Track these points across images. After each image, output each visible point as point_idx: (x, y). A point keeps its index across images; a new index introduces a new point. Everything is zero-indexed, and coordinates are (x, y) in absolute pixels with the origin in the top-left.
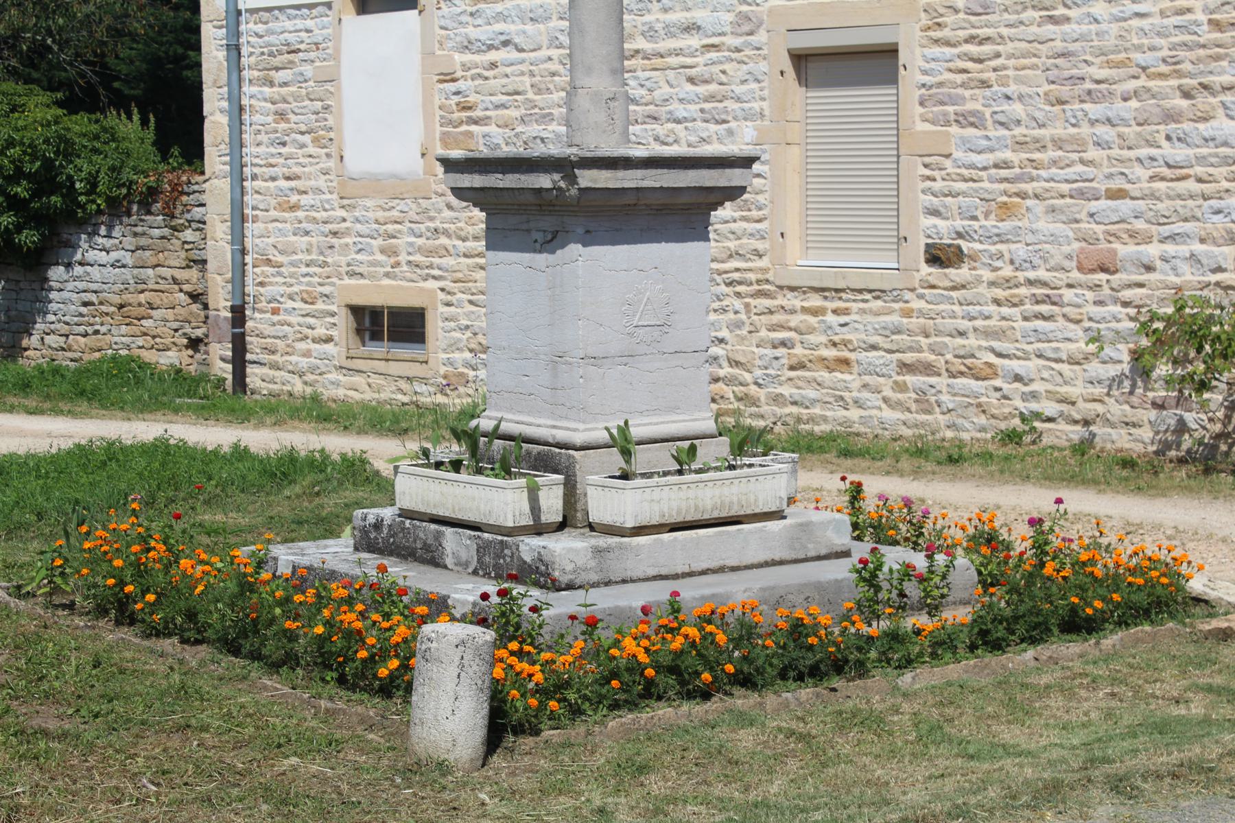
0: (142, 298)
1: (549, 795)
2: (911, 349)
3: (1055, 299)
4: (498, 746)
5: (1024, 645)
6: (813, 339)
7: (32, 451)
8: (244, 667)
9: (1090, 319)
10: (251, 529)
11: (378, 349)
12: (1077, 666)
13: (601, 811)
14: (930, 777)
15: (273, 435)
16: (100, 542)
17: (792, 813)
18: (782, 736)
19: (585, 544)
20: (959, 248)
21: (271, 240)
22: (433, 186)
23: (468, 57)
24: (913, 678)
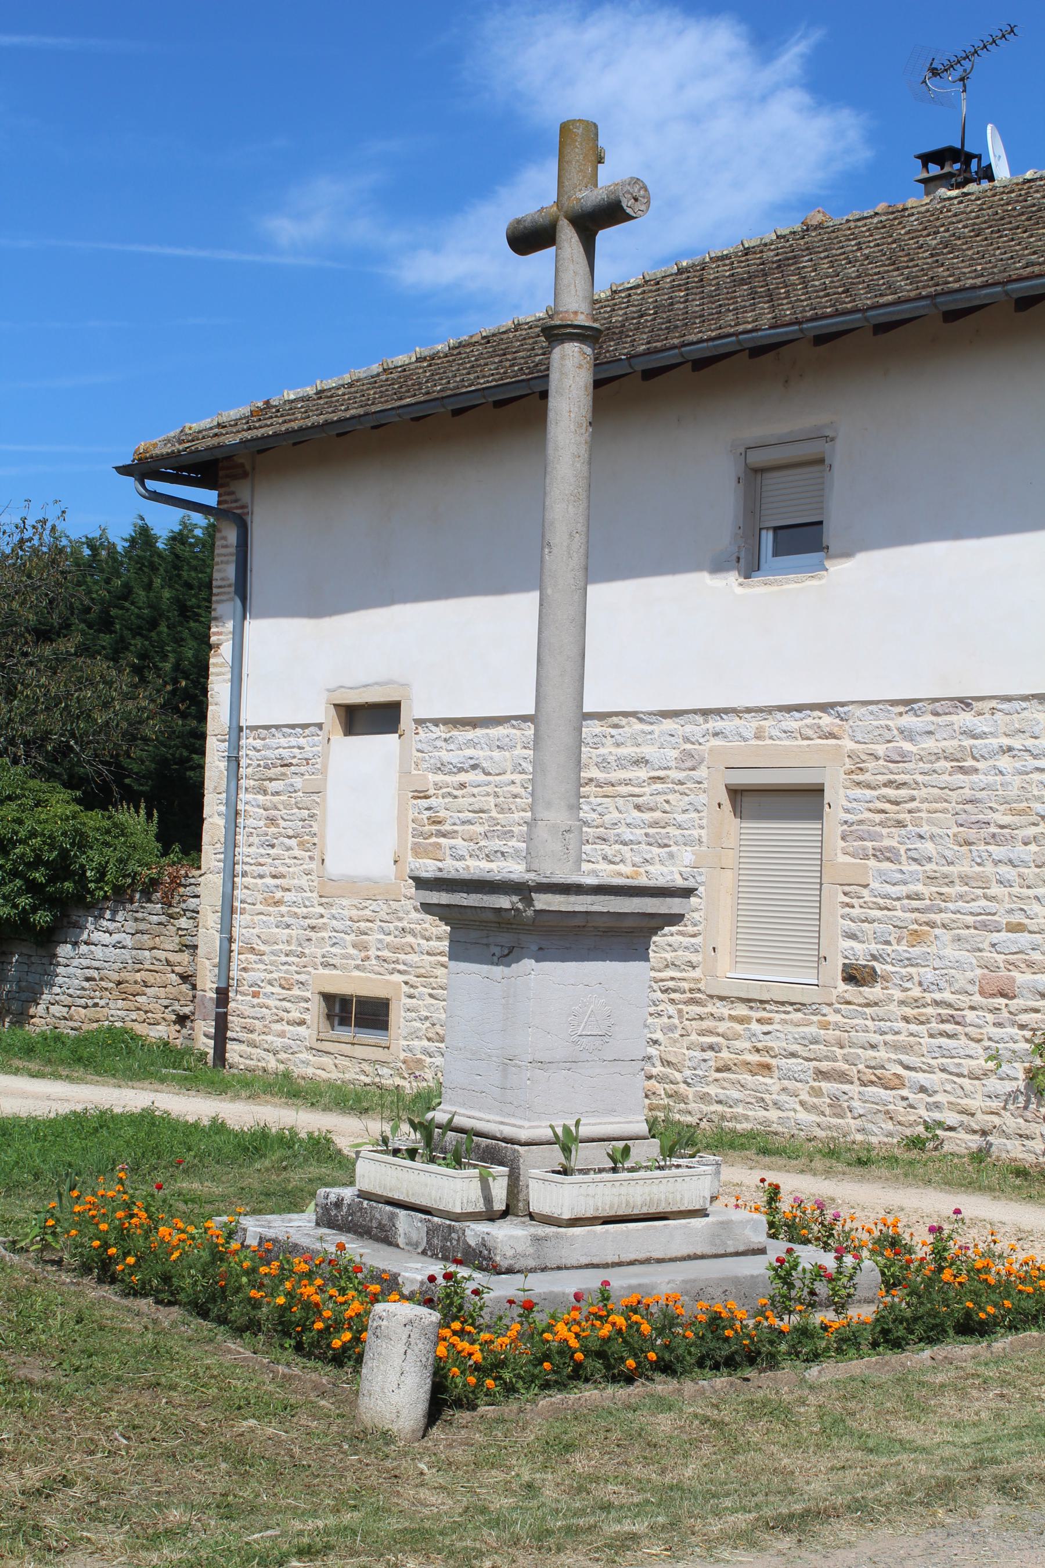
0: (138, 976)
1: (483, 1467)
2: (827, 1058)
3: (959, 1020)
4: (438, 1419)
5: (922, 1344)
6: (738, 1044)
7: (34, 1114)
8: (211, 1330)
9: (990, 1039)
10: (223, 1198)
11: (346, 1033)
12: (970, 1366)
13: (530, 1486)
14: (832, 1469)
15: (247, 1108)
16: (88, 1206)
17: (704, 1498)
18: (697, 1422)
19: (526, 1233)
20: (873, 969)
21: (255, 931)
22: (403, 890)
23: (440, 778)
24: (820, 1372)
